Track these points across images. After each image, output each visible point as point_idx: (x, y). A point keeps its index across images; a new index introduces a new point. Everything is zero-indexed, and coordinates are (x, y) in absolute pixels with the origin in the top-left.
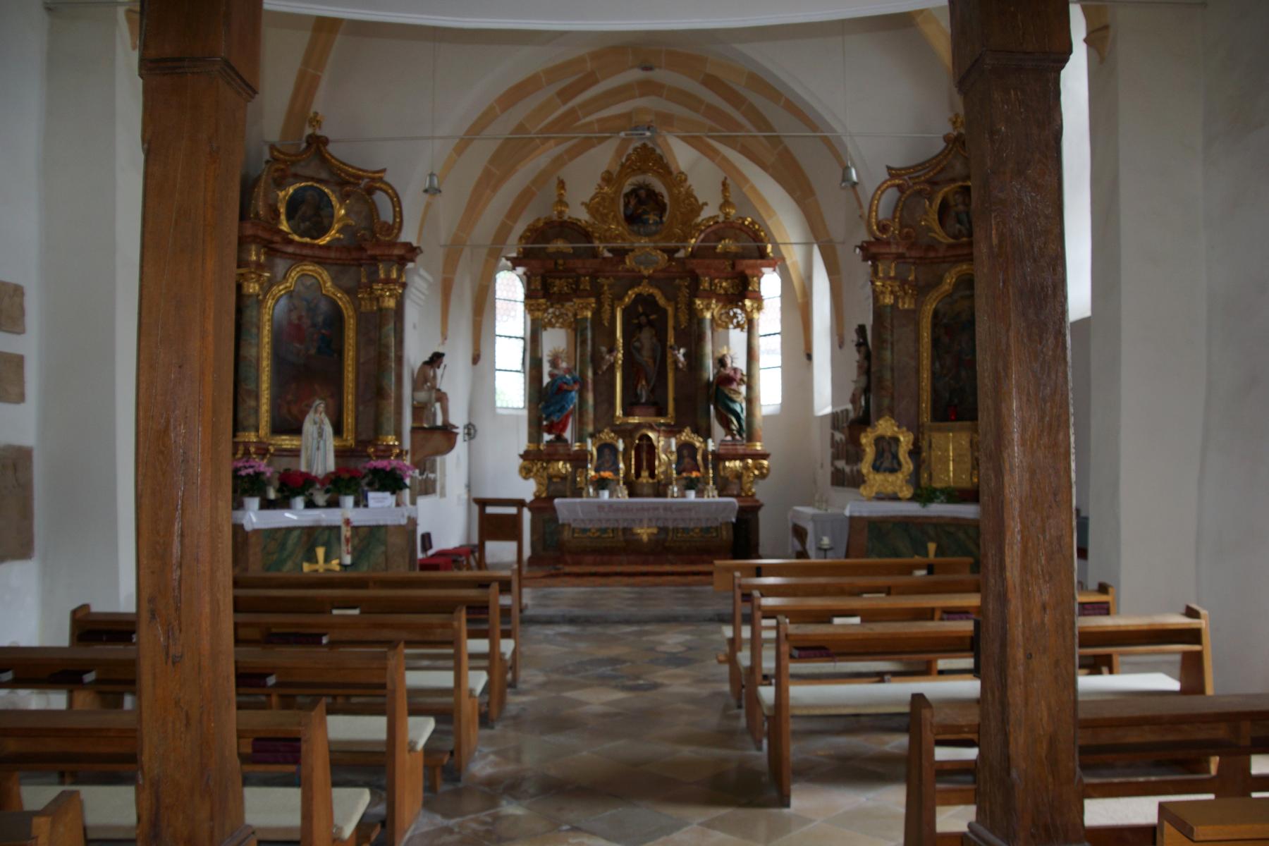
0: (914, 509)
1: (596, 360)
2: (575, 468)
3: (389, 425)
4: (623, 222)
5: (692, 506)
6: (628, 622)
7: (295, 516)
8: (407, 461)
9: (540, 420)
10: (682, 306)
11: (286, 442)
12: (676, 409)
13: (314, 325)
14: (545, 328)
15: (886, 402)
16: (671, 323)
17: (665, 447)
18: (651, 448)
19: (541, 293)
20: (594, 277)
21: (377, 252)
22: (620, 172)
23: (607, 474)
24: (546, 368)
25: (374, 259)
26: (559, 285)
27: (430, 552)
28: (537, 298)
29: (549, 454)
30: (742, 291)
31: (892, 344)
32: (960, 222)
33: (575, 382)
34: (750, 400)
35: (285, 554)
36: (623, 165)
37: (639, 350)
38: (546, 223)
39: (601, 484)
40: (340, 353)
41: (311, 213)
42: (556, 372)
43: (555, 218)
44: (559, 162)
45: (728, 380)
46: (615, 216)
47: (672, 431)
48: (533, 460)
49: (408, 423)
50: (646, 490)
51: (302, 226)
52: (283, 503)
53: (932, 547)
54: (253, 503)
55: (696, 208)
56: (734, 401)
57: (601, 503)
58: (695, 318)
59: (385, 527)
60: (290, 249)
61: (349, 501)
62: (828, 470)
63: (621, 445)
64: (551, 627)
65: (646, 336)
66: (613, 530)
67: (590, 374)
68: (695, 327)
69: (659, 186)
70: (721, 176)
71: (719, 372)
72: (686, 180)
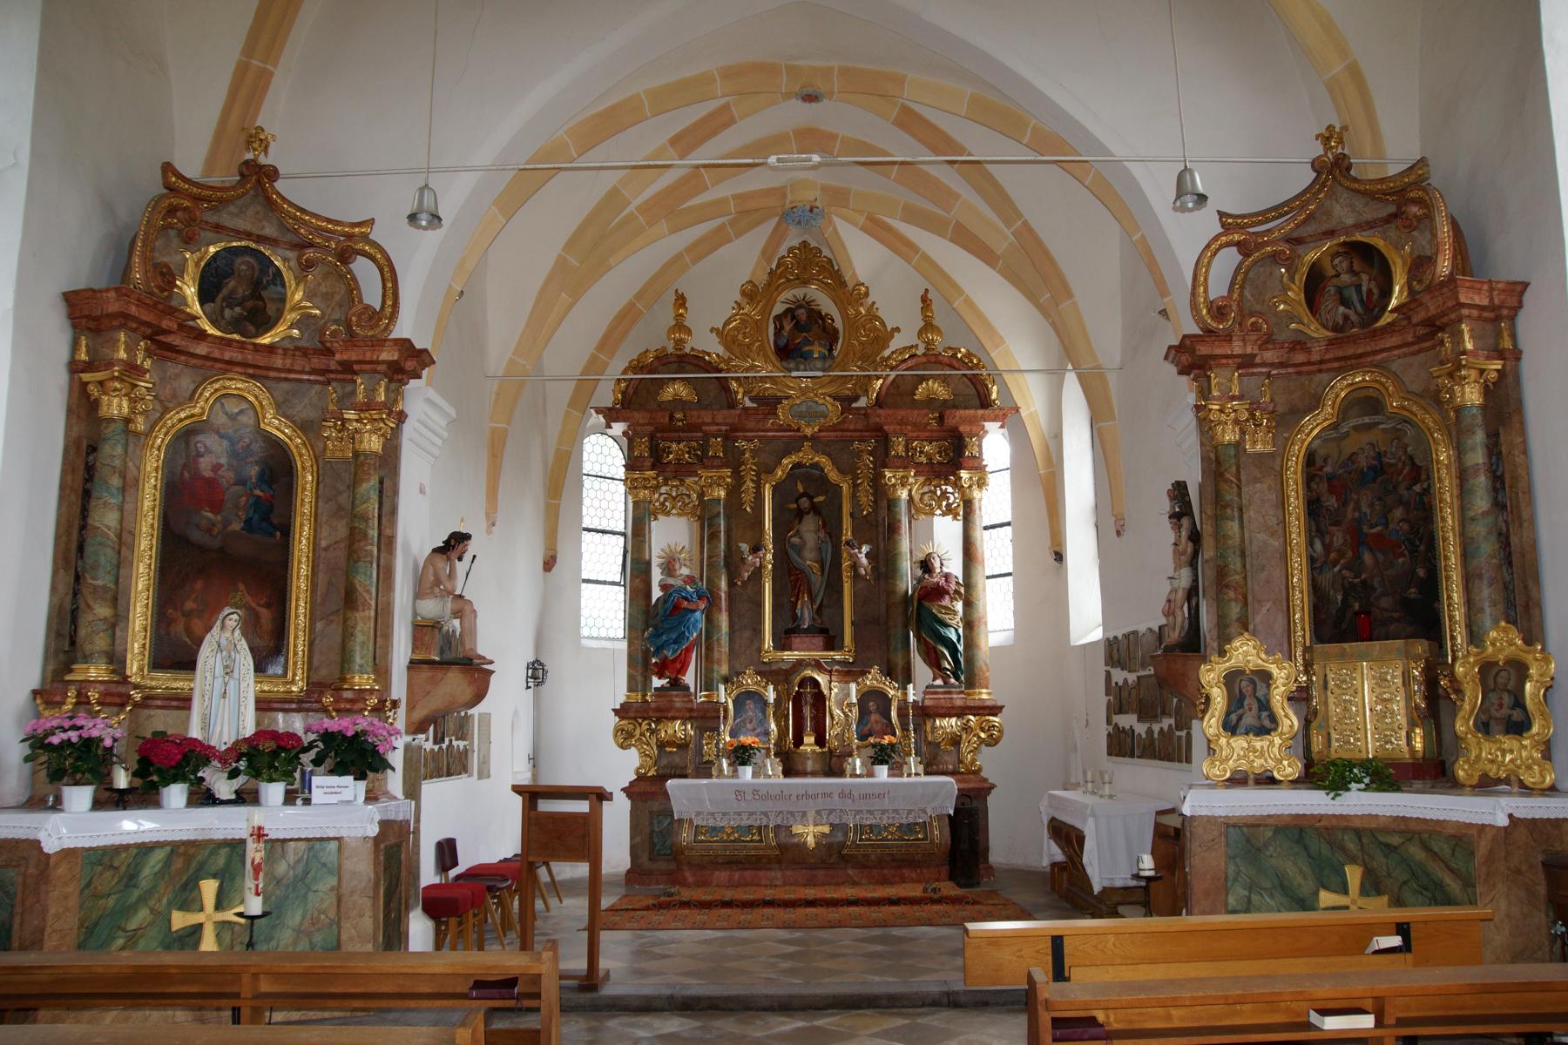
0: (1314, 802)
1: (733, 563)
2: (701, 731)
3: (360, 657)
4: (773, 358)
5: (883, 792)
6: (785, 1006)
7: (173, 819)
8: (400, 719)
9: (646, 656)
10: (865, 485)
11: (165, 681)
12: (856, 638)
13: (241, 482)
14: (654, 514)
15: (1235, 610)
16: (846, 508)
17: (842, 697)
18: (820, 699)
19: (648, 463)
20: (729, 437)
21: (352, 355)
22: (769, 284)
23: (747, 739)
24: (657, 576)
25: (348, 368)
26: (676, 450)
27: (453, 873)
28: (641, 469)
29: (658, 710)
30: (953, 458)
31: (1241, 510)
32: (1345, 302)
33: (700, 598)
34: (969, 624)
35: (136, 893)
36: (771, 273)
37: (799, 550)
38: (657, 358)
39: (741, 755)
40: (286, 530)
41: (244, 293)
42: (671, 581)
43: (670, 350)
44: (676, 264)
45: (938, 592)
46: (762, 348)
47: (850, 672)
48: (634, 717)
49: (401, 650)
51: (228, 313)
52: (143, 796)
53: (1353, 874)
54: (79, 797)
55: (883, 337)
56: (947, 626)
57: (731, 795)
58: (883, 499)
60: (201, 349)
61: (274, 792)
62: (1103, 731)
63: (771, 695)
64: (645, 1019)
65: (809, 530)
67: (723, 585)
68: (884, 512)
69: (827, 305)
70: (920, 285)
71: (920, 580)
72: (867, 294)
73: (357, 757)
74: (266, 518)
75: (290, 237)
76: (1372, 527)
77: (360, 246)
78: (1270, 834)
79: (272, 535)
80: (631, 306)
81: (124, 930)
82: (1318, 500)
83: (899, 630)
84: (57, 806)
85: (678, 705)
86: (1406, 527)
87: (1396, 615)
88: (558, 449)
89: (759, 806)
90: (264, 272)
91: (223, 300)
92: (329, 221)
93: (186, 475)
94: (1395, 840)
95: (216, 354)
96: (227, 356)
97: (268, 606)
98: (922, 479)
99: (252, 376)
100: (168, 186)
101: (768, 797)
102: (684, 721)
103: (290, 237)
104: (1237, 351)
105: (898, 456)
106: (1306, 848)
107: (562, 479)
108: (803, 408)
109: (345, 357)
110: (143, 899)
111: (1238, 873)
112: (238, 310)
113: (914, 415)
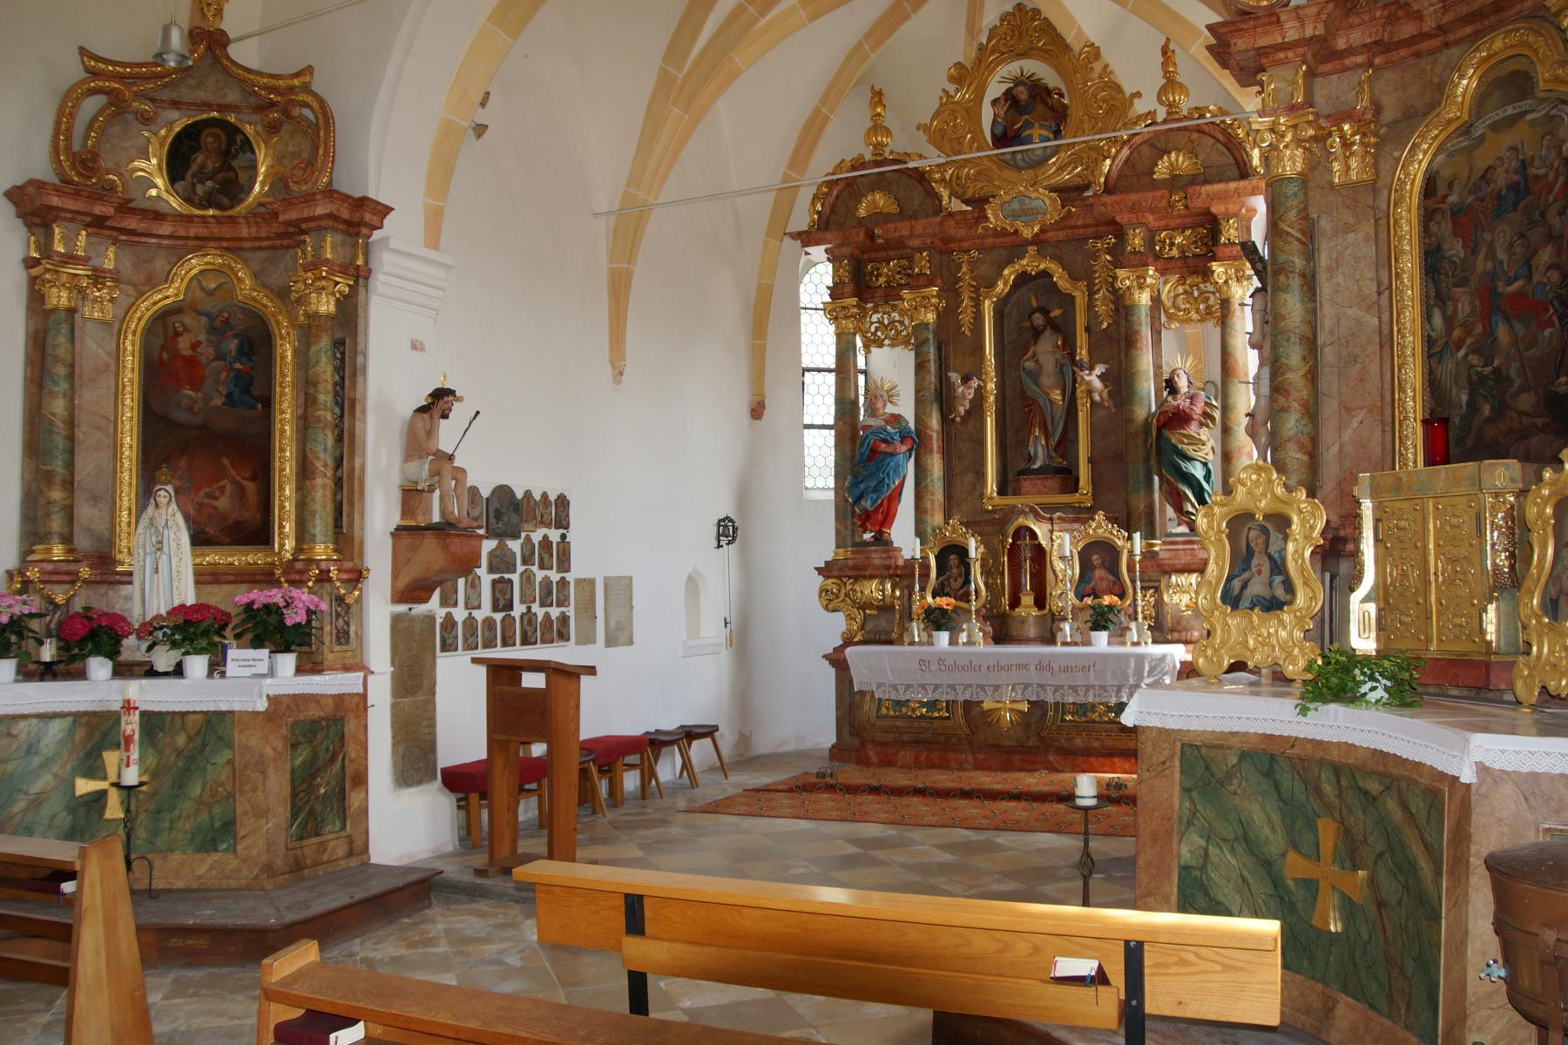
7: (98, 689)
16: (1081, 321)
18: (1040, 554)
21: (293, 215)
29: (854, 568)
35: (36, 761)
36: (981, 48)
39: (937, 620)
40: (267, 402)
45: (1179, 419)
50: (1032, 632)
51: (200, 189)
52: (67, 668)
56: (1190, 459)
58: (1122, 307)
59: (231, 712)
61: (197, 665)
66: (950, 704)
67: (934, 423)
73: (269, 630)
74: (246, 391)
75: (252, 100)
76: (1509, 282)
77: (302, 97)
78: (1234, 760)
79: (253, 407)
80: (816, 113)
81: (26, 793)
82: (1439, 248)
83: (1141, 469)
84: (82, 675)
85: (876, 562)
86: (1555, 276)
87: (1539, 421)
88: (759, 285)
89: (946, 679)
90: (231, 141)
91: (194, 176)
92: (272, 76)
93: (165, 356)
94: (1373, 786)
95: (181, 232)
96: (192, 233)
97: (253, 478)
98: (1174, 278)
99: (228, 249)
100: (87, 70)
101: (955, 667)
102: (883, 579)
103: (252, 100)
104: (1292, 35)
105: (1135, 252)
106: (1277, 786)
107: (767, 319)
108: (1016, 206)
109: (287, 217)
110: (45, 765)
111: (1194, 813)
112: (209, 183)
113: (1149, 197)
